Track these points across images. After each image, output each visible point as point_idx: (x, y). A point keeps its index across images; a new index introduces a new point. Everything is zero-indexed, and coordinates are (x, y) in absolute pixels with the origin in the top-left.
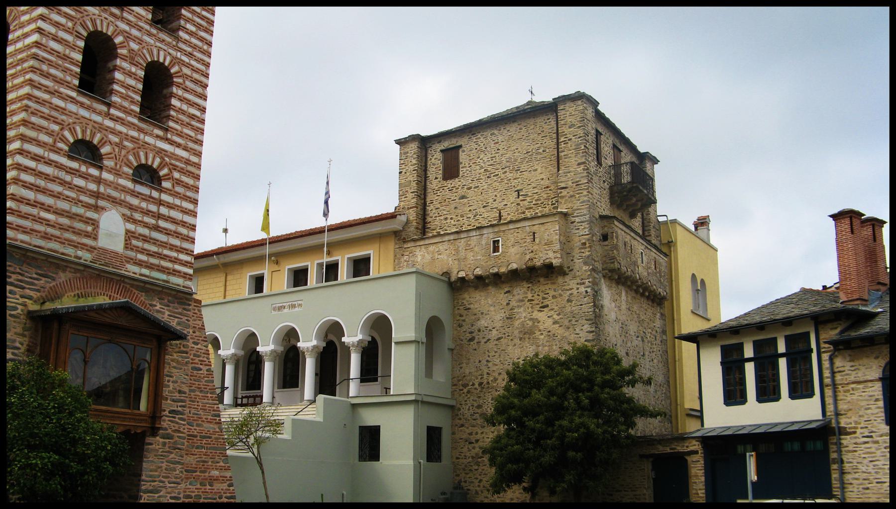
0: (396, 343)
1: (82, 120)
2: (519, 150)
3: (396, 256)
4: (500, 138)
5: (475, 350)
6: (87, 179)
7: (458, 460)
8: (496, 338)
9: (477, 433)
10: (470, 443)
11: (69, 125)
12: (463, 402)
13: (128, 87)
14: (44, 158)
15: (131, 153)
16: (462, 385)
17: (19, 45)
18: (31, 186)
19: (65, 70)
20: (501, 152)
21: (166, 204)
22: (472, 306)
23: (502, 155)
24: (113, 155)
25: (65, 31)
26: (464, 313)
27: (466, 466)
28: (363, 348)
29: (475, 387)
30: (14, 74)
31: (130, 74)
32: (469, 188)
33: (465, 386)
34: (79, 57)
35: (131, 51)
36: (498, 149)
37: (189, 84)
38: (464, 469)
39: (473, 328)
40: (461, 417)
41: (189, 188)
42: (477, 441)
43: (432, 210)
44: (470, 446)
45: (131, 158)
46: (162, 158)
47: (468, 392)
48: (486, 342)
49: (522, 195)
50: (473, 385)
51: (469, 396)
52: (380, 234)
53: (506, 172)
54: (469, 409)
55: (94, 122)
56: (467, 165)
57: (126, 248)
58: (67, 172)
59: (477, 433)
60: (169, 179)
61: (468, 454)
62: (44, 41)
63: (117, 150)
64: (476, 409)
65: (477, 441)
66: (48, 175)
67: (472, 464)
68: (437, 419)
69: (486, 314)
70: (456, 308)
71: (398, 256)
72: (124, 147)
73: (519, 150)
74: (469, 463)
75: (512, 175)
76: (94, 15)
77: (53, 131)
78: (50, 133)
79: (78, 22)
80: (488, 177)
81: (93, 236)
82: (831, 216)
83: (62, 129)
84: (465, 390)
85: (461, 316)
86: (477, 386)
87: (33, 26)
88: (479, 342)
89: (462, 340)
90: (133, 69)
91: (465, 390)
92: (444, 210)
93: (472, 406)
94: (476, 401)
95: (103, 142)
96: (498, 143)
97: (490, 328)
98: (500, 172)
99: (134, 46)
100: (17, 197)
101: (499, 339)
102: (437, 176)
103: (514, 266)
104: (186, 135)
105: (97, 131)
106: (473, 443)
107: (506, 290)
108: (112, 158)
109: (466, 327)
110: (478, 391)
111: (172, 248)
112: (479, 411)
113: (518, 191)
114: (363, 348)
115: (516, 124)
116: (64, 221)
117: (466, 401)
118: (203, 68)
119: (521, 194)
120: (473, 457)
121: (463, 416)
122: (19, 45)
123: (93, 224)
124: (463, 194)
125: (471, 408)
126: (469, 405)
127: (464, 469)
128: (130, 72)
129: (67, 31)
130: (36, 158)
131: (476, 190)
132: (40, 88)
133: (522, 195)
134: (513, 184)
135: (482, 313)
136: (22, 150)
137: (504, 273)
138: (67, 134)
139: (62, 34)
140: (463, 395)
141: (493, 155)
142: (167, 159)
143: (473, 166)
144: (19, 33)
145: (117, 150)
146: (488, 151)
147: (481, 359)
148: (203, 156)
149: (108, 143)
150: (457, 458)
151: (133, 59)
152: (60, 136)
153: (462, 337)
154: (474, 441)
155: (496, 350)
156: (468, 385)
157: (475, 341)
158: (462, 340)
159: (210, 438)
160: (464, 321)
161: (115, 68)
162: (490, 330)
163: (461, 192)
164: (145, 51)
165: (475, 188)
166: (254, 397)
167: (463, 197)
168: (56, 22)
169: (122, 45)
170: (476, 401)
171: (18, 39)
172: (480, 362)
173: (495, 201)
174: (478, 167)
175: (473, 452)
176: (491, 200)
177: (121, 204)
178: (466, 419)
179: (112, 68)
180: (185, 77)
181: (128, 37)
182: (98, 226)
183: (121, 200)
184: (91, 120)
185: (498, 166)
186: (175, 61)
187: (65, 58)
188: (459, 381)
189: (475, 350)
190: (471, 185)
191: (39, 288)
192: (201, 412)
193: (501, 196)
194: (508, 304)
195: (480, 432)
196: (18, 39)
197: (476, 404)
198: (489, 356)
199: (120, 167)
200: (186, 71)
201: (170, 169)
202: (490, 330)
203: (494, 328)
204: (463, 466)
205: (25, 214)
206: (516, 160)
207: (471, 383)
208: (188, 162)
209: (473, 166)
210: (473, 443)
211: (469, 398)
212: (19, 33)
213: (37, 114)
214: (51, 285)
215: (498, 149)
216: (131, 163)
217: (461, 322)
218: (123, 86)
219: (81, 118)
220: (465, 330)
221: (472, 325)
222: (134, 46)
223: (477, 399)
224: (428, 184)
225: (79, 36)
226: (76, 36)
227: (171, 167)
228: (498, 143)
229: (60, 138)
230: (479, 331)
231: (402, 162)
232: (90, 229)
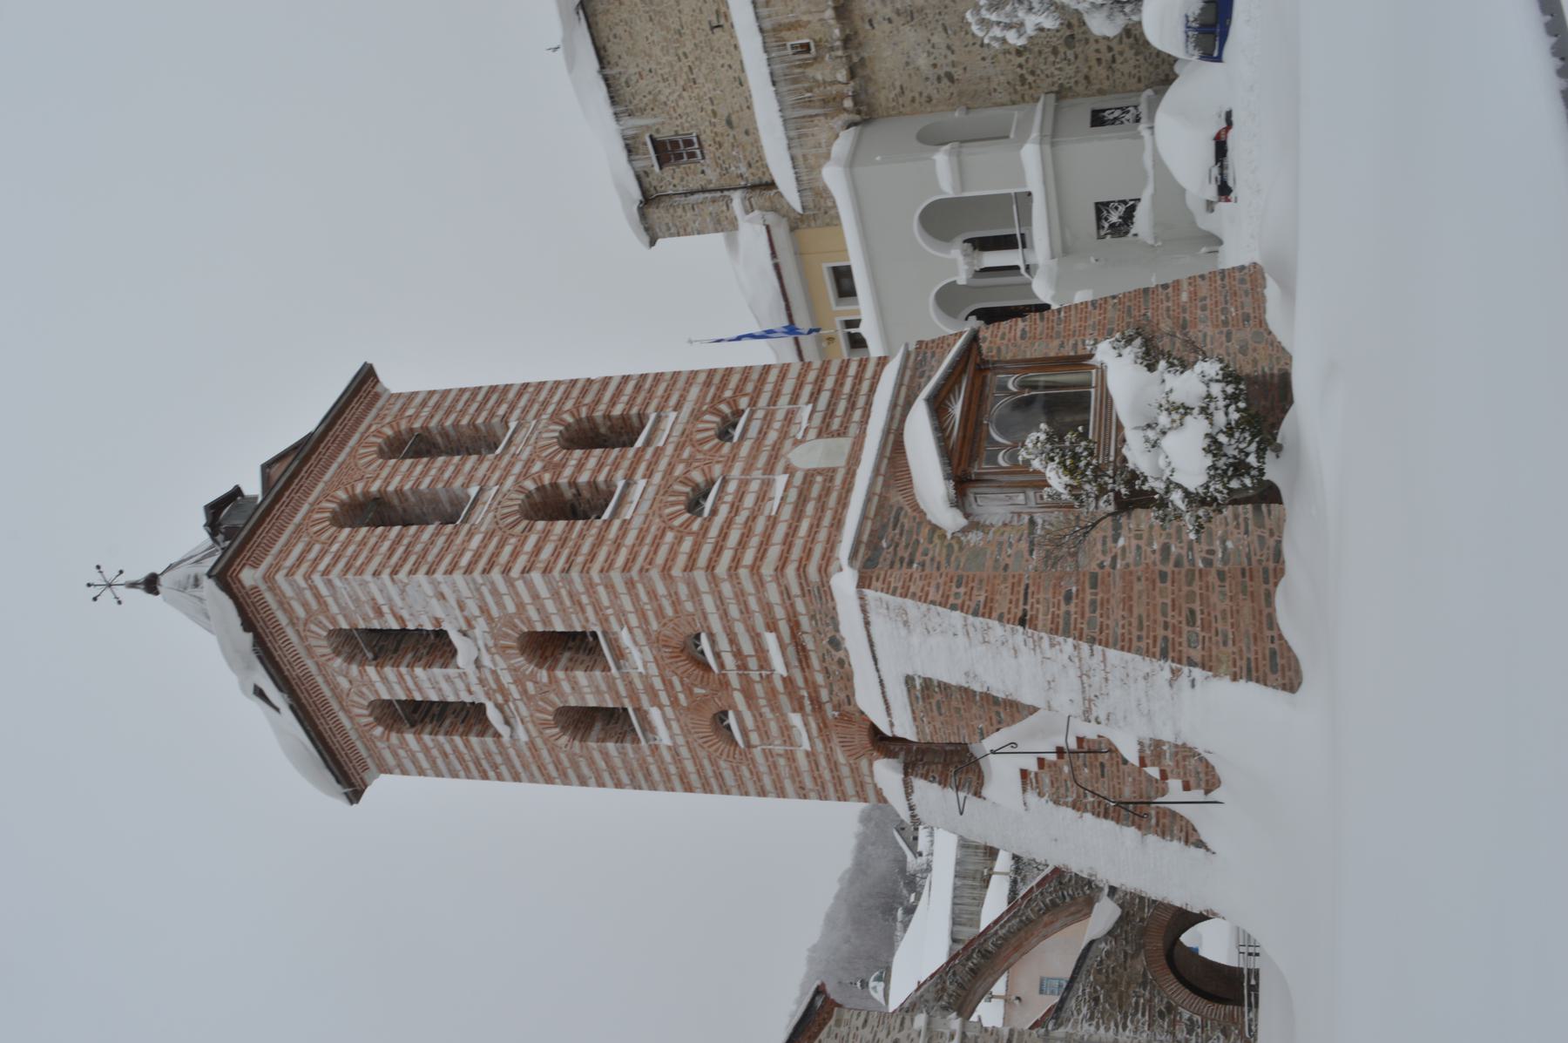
0: (963, 188)
1: (656, 505)
2: (648, 34)
3: (828, 225)
4: (632, 70)
5: (965, 69)
6: (743, 493)
7: (1143, 79)
8: (945, 35)
9: (1098, 51)
10: (1114, 60)
11: (664, 522)
12: (1050, 80)
13: (600, 466)
14: (717, 542)
15: (700, 448)
16: (1023, 85)
17: (550, 606)
18: (762, 551)
19: (582, 536)
20: (653, 66)
21: (772, 461)
22: (898, 84)
23: (659, 63)
24: (706, 467)
25: (523, 544)
26: (909, 95)
27: (1151, 64)
28: (975, 249)
29: (1023, 63)
30: (594, 606)
31: (580, 467)
32: (714, 114)
33: (1023, 79)
34: (560, 525)
35: (545, 469)
36: (650, 71)
37: (588, 399)
38: (1157, 67)
39: (930, 76)
40: (1073, 80)
41: (746, 377)
42: (1110, 49)
43: (753, 174)
44: (1119, 59)
45: (707, 447)
46: (704, 413)
47: (1033, 73)
48: (953, 52)
49: (718, 21)
50: (1020, 66)
51: (1038, 72)
52: (796, 253)
53: (685, 55)
54: (1060, 69)
55: (657, 494)
56: (678, 122)
57: (844, 433)
58: (736, 515)
59: (1098, 51)
60: (734, 401)
61: (1132, 62)
62: (541, 565)
63: (697, 464)
64: (1059, 57)
65: (1110, 49)
66: (743, 534)
67: (1147, 54)
68: (1080, 112)
69: (909, 57)
70: (902, 109)
71: (828, 220)
72: (691, 456)
73: (648, 34)
74: (1145, 59)
75: (687, 43)
76: (495, 517)
77: (676, 538)
78: (680, 540)
79: (508, 532)
80: (695, 83)
81: (830, 474)
82: (355, 795)
83: (671, 528)
84: (1030, 79)
85: (913, 100)
86: (1022, 60)
87: (520, 585)
88: (954, 64)
89: (952, 94)
90: (573, 462)
91: (1030, 79)
92: (751, 152)
93: (1054, 63)
94: (1046, 58)
95: (685, 480)
96: (640, 74)
97: (928, 47)
98: (686, 63)
99: (537, 466)
100: (780, 564)
101: (945, 30)
102: (700, 171)
103: (829, 13)
104: (665, 391)
105: (671, 489)
106: (1113, 56)
107: (867, 27)
108: (710, 468)
109: (930, 89)
110: (1031, 56)
111: (839, 383)
112: (1062, 49)
113: (713, 28)
114: (975, 249)
115: (608, 45)
116: (810, 508)
117: (1047, 76)
118: (562, 389)
119: (715, 23)
120: (1137, 54)
121: (1070, 78)
122: (550, 606)
123: (813, 475)
124: (724, 122)
125: (1058, 66)
126: (1053, 69)
127: (1157, 67)
128: (577, 465)
129: (523, 542)
130: (718, 550)
131: (715, 102)
132: (612, 560)
133: (718, 21)
134: (703, 38)
135: (907, 64)
136: (708, 567)
137: (842, 30)
138: (677, 522)
139: (529, 546)
140: (1038, 81)
141: (660, 79)
142: (705, 408)
143: (679, 111)
144: (532, 613)
145: (697, 464)
146: (655, 88)
147: (979, 58)
148: (696, 369)
149: (687, 475)
150: (1139, 80)
151: (556, 465)
152: (682, 529)
153: (948, 94)
154: (1111, 54)
155: (963, 33)
156: (1022, 76)
157: (953, 70)
158: (952, 94)
159: (1129, 307)
160: (921, 94)
161: (573, 484)
162: (933, 47)
163: (721, 127)
164: (544, 454)
165: (712, 103)
166: (1057, 629)
167: (729, 123)
168: (511, 555)
169: (537, 478)
170: (1046, 58)
171: (541, 610)
172: (983, 59)
173: (730, 66)
174: (681, 103)
175: (1129, 54)
176: (731, 73)
177: (779, 449)
178: (1077, 72)
179: (574, 491)
180: (577, 405)
181: (525, 474)
182: (815, 470)
183: (773, 449)
184: (655, 499)
185: (676, 68)
186: (555, 418)
187: (563, 541)
188: (1016, 91)
189: (965, 69)
190: (709, 112)
191: (915, 524)
192: (1090, 322)
193: (723, 57)
194: (890, 21)
195: (1095, 46)
196: (541, 610)
197: (1052, 58)
198: (974, 44)
199: (721, 457)
200: (569, 405)
201: (720, 402)
202: (933, 47)
203: (929, 41)
204: (1151, 69)
205: (804, 552)
206: (665, 39)
207: (1018, 70)
208: (707, 384)
209: (679, 111)
210: (1113, 56)
211: (1042, 71)
212: (532, 613)
213: (652, 559)
214: (910, 511)
215: (650, 71)
216: (715, 446)
217: (924, 99)
218: (599, 471)
219: (654, 508)
220: (935, 91)
221: (927, 79)
222: (537, 466)
223: (1043, 56)
224: (711, 186)
225: (529, 529)
226: (530, 530)
227: (716, 401)
228: (640, 74)
229: (686, 528)
230: (935, 66)
231: (682, 231)
232: (819, 479)
